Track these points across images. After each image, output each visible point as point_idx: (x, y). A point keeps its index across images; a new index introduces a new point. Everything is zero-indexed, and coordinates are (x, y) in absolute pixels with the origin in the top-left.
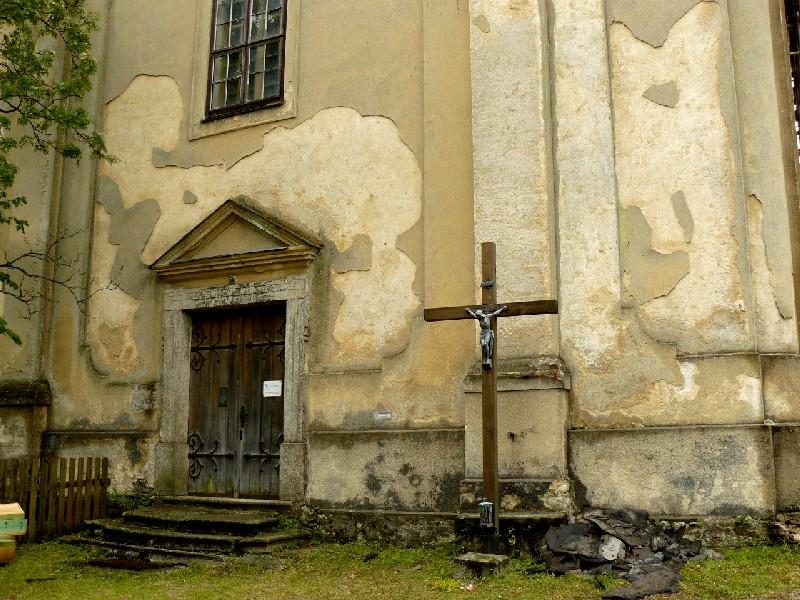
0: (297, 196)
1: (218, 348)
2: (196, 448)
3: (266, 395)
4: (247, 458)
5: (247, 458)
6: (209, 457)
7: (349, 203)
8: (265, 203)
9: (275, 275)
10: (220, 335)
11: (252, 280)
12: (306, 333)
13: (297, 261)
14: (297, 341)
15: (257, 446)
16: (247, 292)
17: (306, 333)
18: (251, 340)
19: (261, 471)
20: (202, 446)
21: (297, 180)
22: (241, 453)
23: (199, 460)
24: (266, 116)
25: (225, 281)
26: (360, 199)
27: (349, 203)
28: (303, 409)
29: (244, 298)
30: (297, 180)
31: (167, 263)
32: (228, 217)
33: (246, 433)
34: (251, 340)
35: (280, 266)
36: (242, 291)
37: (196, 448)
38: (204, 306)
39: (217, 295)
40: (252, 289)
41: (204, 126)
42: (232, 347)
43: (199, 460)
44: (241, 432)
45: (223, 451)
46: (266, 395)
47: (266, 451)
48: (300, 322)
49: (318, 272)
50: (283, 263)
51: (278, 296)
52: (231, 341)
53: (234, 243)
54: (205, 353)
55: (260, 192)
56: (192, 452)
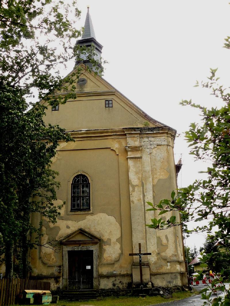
7: (106, 232)
8: (87, 230)
21: (94, 226)
24: (86, 212)
26: (108, 232)
27: (106, 232)
30: (94, 226)
41: (71, 212)
55: (85, 228)
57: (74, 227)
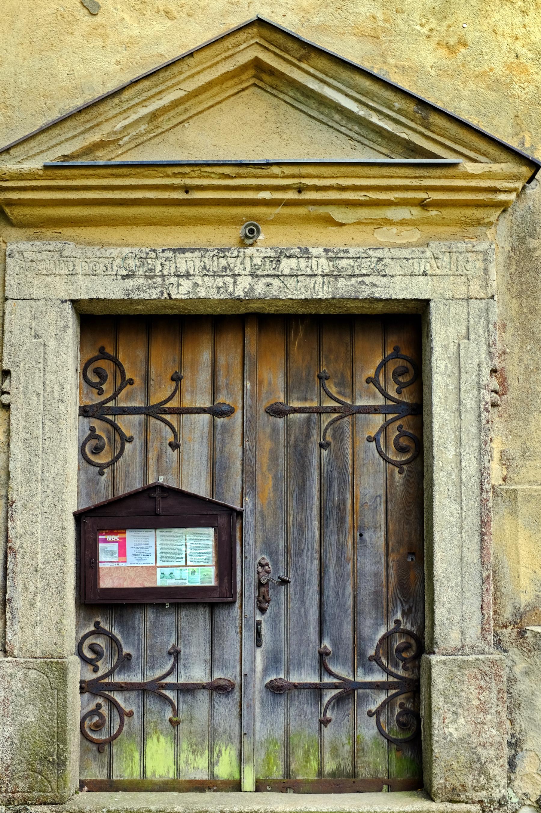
0: (443, 52)
1: (171, 411)
2: (104, 667)
3: (211, 531)
4: (276, 690)
5: (276, 690)
6: (150, 690)
9: (384, 235)
10: (177, 379)
11: (318, 239)
12: (494, 384)
13: (467, 204)
14: (469, 402)
15: (312, 658)
16: (304, 267)
17: (494, 384)
18: (281, 398)
19: (324, 722)
20: (124, 662)
22: (259, 679)
23: (118, 697)
25: (232, 234)
28: (491, 576)
29: (291, 282)
31: (35, 165)
32: (243, 68)
33: (274, 627)
34: (281, 398)
35: (416, 212)
36: (286, 265)
37: (104, 667)
38: (154, 294)
39: (196, 269)
40: (325, 265)
42: (217, 412)
43: (118, 697)
44: (259, 623)
45: (197, 673)
46: (211, 531)
47: (335, 670)
48: (477, 355)
49: (522, 240)
50: (423, 205)
51: (400, 288)
52: (215, 391)
53: (243, 132)
54: (129, 424)
56: (91, 676)
57: (168, 14)
